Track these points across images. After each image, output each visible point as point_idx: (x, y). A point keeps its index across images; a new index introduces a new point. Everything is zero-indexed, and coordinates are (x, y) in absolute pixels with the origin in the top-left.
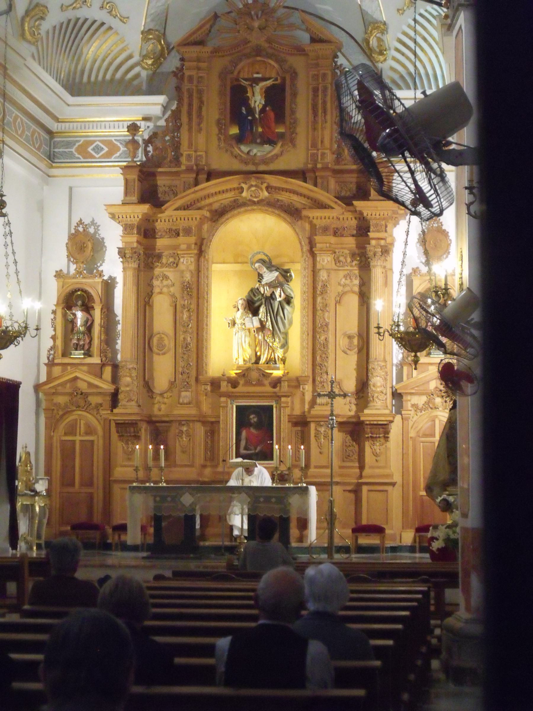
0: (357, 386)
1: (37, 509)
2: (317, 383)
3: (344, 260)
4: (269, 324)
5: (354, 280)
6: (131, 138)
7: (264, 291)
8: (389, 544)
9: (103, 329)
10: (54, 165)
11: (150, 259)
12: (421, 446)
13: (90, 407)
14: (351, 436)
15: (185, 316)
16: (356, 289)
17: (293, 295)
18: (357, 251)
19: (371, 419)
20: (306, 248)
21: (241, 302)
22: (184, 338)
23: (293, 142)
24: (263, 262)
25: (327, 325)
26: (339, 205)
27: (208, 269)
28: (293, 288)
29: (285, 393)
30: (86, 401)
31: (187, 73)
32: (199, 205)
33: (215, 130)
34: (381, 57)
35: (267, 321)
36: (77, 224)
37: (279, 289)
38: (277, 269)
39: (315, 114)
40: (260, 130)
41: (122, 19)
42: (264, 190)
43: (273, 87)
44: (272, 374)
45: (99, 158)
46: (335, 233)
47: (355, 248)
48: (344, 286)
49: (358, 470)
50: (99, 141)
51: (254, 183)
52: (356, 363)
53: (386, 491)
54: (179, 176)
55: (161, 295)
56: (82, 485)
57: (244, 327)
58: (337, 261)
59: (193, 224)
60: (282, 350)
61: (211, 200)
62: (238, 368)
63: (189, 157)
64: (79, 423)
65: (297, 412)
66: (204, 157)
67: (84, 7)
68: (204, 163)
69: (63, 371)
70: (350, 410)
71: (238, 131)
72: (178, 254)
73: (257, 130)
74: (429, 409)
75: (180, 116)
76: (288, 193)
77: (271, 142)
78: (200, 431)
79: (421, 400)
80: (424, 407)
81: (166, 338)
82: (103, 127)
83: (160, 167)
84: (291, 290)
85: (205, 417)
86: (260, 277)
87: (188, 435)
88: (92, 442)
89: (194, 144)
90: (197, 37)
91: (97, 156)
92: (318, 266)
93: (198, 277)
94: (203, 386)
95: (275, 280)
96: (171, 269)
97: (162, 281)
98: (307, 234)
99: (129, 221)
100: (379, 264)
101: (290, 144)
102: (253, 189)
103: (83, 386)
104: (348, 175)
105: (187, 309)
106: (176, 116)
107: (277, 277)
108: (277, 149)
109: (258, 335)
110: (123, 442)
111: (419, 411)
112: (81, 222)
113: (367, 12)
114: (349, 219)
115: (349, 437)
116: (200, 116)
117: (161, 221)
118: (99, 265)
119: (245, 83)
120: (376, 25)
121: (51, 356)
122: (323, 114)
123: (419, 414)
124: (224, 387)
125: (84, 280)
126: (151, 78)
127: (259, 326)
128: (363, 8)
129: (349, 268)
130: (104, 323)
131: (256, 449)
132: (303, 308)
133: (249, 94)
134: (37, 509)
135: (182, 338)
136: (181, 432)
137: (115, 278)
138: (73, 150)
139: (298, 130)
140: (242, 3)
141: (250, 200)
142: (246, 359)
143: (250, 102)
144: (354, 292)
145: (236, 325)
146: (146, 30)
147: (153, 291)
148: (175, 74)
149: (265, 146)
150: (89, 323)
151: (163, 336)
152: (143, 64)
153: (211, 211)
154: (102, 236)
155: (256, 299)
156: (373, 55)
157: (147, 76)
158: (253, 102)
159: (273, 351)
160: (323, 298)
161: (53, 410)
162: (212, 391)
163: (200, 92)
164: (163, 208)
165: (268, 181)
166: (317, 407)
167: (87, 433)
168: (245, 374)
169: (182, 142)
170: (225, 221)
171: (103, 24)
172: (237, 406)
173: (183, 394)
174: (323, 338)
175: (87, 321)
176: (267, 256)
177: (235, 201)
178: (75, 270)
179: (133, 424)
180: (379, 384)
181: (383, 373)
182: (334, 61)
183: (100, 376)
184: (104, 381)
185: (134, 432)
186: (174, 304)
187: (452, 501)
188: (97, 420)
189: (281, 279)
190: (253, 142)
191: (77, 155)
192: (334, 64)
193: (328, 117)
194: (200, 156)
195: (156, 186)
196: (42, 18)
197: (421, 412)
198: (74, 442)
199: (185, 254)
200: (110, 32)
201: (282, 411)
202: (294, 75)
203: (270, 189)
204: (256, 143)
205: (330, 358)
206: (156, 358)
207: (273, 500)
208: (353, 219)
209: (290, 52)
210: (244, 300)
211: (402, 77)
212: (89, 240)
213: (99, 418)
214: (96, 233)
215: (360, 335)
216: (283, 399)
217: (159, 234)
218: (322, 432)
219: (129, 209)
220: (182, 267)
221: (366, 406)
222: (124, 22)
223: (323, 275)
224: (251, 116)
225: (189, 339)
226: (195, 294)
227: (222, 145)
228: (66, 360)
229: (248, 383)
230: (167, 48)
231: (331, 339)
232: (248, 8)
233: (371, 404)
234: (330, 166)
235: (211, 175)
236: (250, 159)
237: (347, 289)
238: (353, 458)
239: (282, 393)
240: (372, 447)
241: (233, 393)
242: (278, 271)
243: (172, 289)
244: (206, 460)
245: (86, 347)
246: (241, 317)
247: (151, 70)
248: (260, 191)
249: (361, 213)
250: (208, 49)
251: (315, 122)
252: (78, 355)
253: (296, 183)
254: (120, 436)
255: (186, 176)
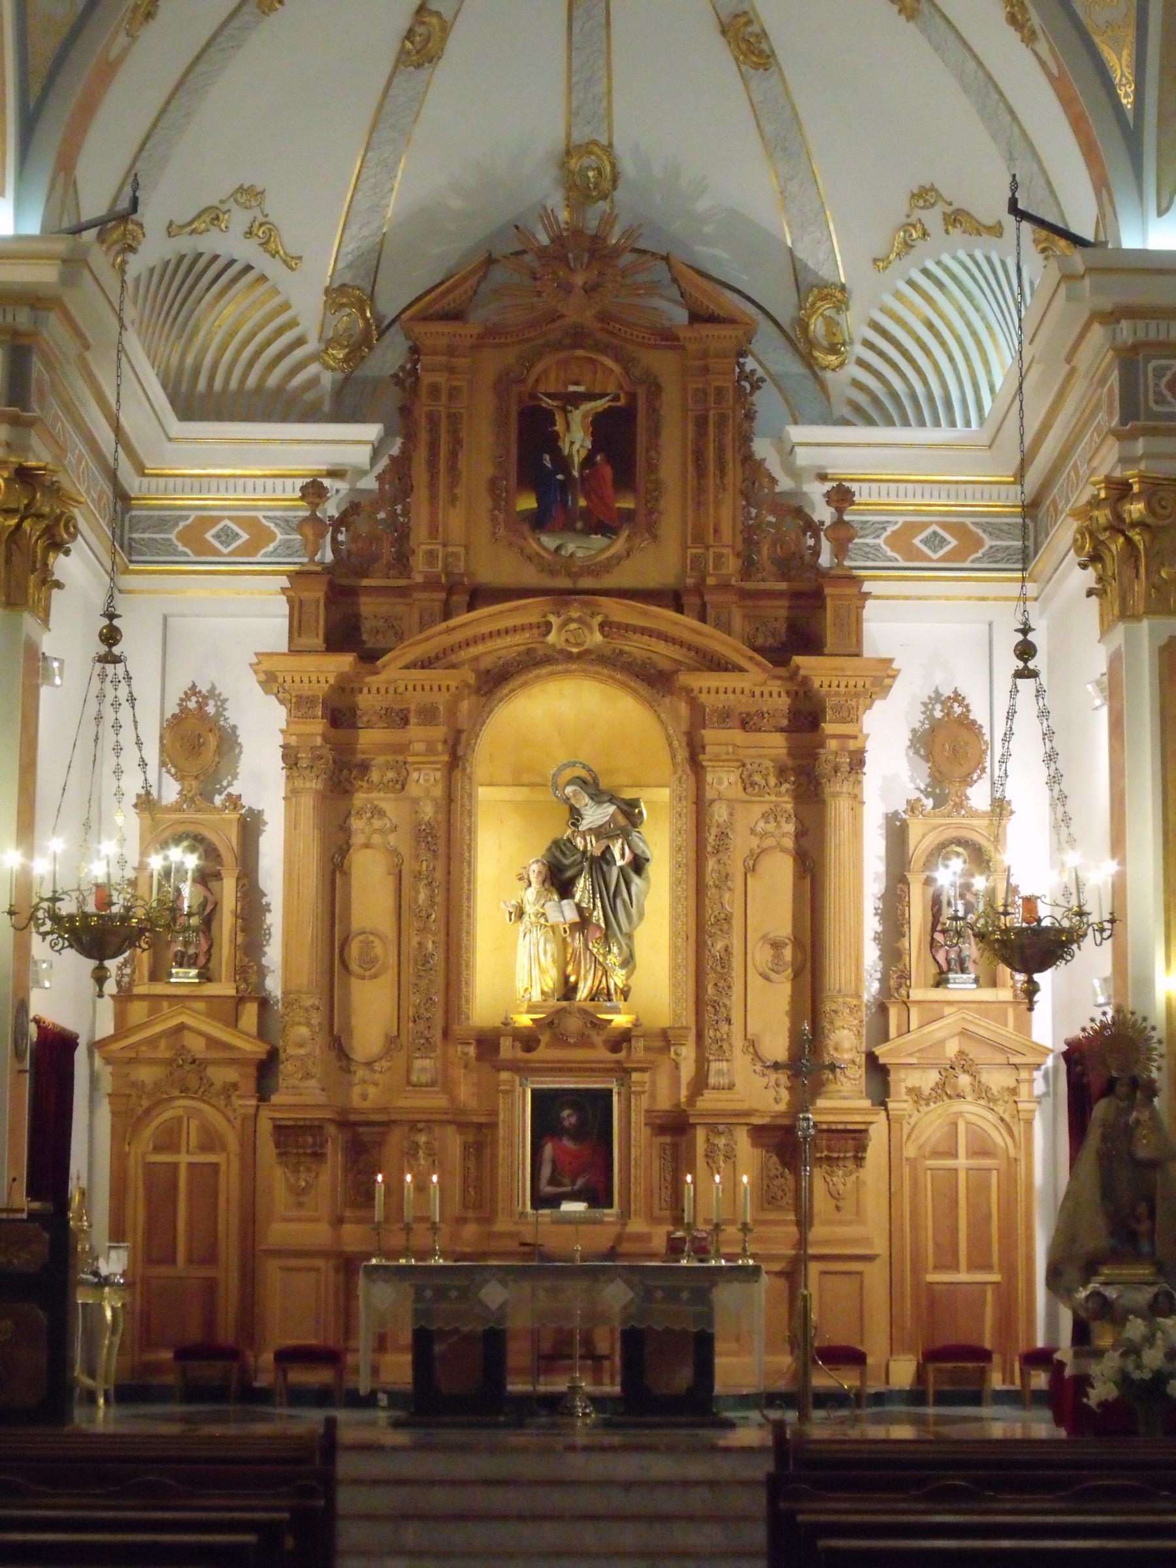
0: (790, 1049)
1: (109, 1314)
2: (708, 1041)
3: (763, 783)
4: (598, 914)
5: (783, 823)
6: (307, 514)
7: (586, 846)
8: (873, 1387)
9: (240, 921)
10: (132, 567)
11: (345, 772)
12: (929, 1178)
13: (212, 1090)
14: (778, 1155)
15: (422, 896)
16: (789, 843)
17: (649, 856)
18: (790, 763)
19: (831, 1118)
20: (682, 754)
21: (535, 867)
22: (420, 943)
23: (651, 529)
24: (582, 783)
25: (728, 919)
26: (758, 664)
27: (470, 795)
28: (647, 840)
29: (640, 1062)
30: (201, 1079)
31: (427, 379)
32: (453, 658)
33: (485, 503)
34: (833, 358)
35: (594, 909)
36: (186, 693)
37: (620, 841)
38: (612, 800)
39: (701, 472)
40: (582, 502)
41: (289, 259)
42: (596, 627)
43: (609, 412)
44: (611, 1021)
45: (231, 554)
46: (745, 724)
47: (786, 757)
48: (764, 835)
49: (793, 1230)
50: (230, 518)
51: (575, 614)
52: (788, 999)
53: (860, 1273)
54: (411, 596)
55: (368, 851)
56: (190, 1261)
57: (542, 921)
58: (747, 784)
59: (441, 700)
60: (624, 972)
61: (480, 649)
62: (532, 1009)
63: (431, 555)
64: (185, 1129)
65: (664, 1103)
66: (463, 558)
67: (215, 231)
68: (462, 571)
69: (153, 1011)
70: (777, 1101)
71: (535, 505)
72: (405, 763)
73: (575, 501)
74: (945, 1098)
75: (409, 469)
76: (646, 637)
77: (606, 529)
78: (454, 1143)
79: (928, 1080)
80: (934, 1094)
81: (377, 942)
82: (240, 488)
83: (367, 577)
84: (644, 841)
85: (463, 1112)
86: (575, 815)
87: (431, 1153)
88: (215, 1166)
89: (440, 529)
90: (448, 303)
91: (226, 551)
92: (710, 794)
93: (449, 812)
94: (459, 1048)
95: (609, 822)
96: (391, 795)
97: (369, 819)
98: (684, 726)
99: (306, 690)
100: (844, 790)
101: (647, 535)
102: (573, 626)
103: (196, 1045)
104: (770, 603)
105: (425, 882)
106: (399, 470)
107: (613, 815)
108: (619, 544)
109: (573, 939)
110: (287, 1167)
111: (923, 1102)
112: (193, 690)
113: (806, 265)
114: (775, 695)
115: (775, 1159)
116: (453, 469)
117: (369, 691)
118: (225, 783)
119: (548, 403)
120: (825, 291)
121: (126, 979)
122: (718, 473)
123: (924, 1109)
124: (508, 1049)
125: (199, 816)
126: (340, 390)
127: (577, 919)
128: (800, 255)
129: (773, 798)
130: (242, 909)
131: (573, 1183)
132: (676, 883)
133: (559, 427)
134: (109, 1314)
135: (415, 941)
136: (416, 1146)
137: (260, 813)
138: (172, 536)
139: (663, 504)
140: (548, 233)
141: (562, 651)
142: (546, 989)
143: (560, 444)
144: (783, 850)
145: (526, 918)
146: (335, 286)
147: (351, 842)
148: (397, 380)
149: (594, 536)
150: (208, 910)
151: (372, 938)
152: (327, 358)
153: (477, 672)
154: (232, 722)
155: (567, 862)
156: (816, 354)
157: (333, 382)
158: (567, 445)
159: (605, 972)
160: (719, 861)
161: (130, 1096)
162: (480, 1057)
163: (454, 419)
164: (379, 663)
165: (604, 610)
166: (708, 1094)
167: (204, 1148)
168: (551, 1024)
169: (412, 524)
170: (507, 695)
171: (248, 268)
172: (534, 1091)
173: (418, 1064)
174: (720, 945)
175: (203, 905)
176: (590, 770)
177: (529, 652)
178: (180, 793)
179: (315, 1129)
180: (846, 1045)
181: (856, 1022)
182: (738, 364)
183: (233, 1022)
184: (240, 1031)
185: (314, 1144)
186: (396, 871)
187: (1114, 1296)
188: (229, 1120)
189: (622, 821)
190: (568, 527)
191: (181, 548)
192: (737, 370)
193: (729, 479)
194: (453, 554)
195: (357, 616)
196: (132, 249)
197: (928, 1105)
198: (175, 1166)
199: (422, 763)
200: (262, 288)
201: (633, 1100)
202: (655, 390)
203: (607, 629)
204: (574, 530)
205: (734, 989)
206: (355, 983)
207: (685, 1295)
208: (783, 694)
209: (646, 341)
210: (543, 864)
211: (875, 400)
212: (210, 730)
213: (230, 1114)
214: (219, 714)
215: (797, 942)
216: (635, 1076)
217: (365, 719)
218: (721, 1146)
219: (309, 662)
220: (414, 790)
221: (819, 1089)
222: (292, 269)
223: (720, 813)
224: (562, 473)
225: (430, 945)
226: (442, 850)
227: (502, 532)
228: (159, 989)
229: (560, 1040)
230: (377, 327)
231: (737, 950)
232: (562, 246)
233: (831, 1087)
234: (733, 582)
235: (479, 596)
236: (558, 564)
237: (769, 842)
238: (783, 1203)
239: (633, 1062)
240: (828, 1179)
241: (527, 1061)
242: (613, 803)
243: (392, 838)
244: (465, 1207)
245: (202, 960)
246: (537, 900)
247: (343, 371)
248: (586, 631)
249: (806, 681)
250: (471, 328)
251: (700, 490)
252: (184, 976)
253: (665, 617)
254: (280, 1155)
255: (424, 595)
